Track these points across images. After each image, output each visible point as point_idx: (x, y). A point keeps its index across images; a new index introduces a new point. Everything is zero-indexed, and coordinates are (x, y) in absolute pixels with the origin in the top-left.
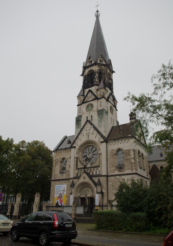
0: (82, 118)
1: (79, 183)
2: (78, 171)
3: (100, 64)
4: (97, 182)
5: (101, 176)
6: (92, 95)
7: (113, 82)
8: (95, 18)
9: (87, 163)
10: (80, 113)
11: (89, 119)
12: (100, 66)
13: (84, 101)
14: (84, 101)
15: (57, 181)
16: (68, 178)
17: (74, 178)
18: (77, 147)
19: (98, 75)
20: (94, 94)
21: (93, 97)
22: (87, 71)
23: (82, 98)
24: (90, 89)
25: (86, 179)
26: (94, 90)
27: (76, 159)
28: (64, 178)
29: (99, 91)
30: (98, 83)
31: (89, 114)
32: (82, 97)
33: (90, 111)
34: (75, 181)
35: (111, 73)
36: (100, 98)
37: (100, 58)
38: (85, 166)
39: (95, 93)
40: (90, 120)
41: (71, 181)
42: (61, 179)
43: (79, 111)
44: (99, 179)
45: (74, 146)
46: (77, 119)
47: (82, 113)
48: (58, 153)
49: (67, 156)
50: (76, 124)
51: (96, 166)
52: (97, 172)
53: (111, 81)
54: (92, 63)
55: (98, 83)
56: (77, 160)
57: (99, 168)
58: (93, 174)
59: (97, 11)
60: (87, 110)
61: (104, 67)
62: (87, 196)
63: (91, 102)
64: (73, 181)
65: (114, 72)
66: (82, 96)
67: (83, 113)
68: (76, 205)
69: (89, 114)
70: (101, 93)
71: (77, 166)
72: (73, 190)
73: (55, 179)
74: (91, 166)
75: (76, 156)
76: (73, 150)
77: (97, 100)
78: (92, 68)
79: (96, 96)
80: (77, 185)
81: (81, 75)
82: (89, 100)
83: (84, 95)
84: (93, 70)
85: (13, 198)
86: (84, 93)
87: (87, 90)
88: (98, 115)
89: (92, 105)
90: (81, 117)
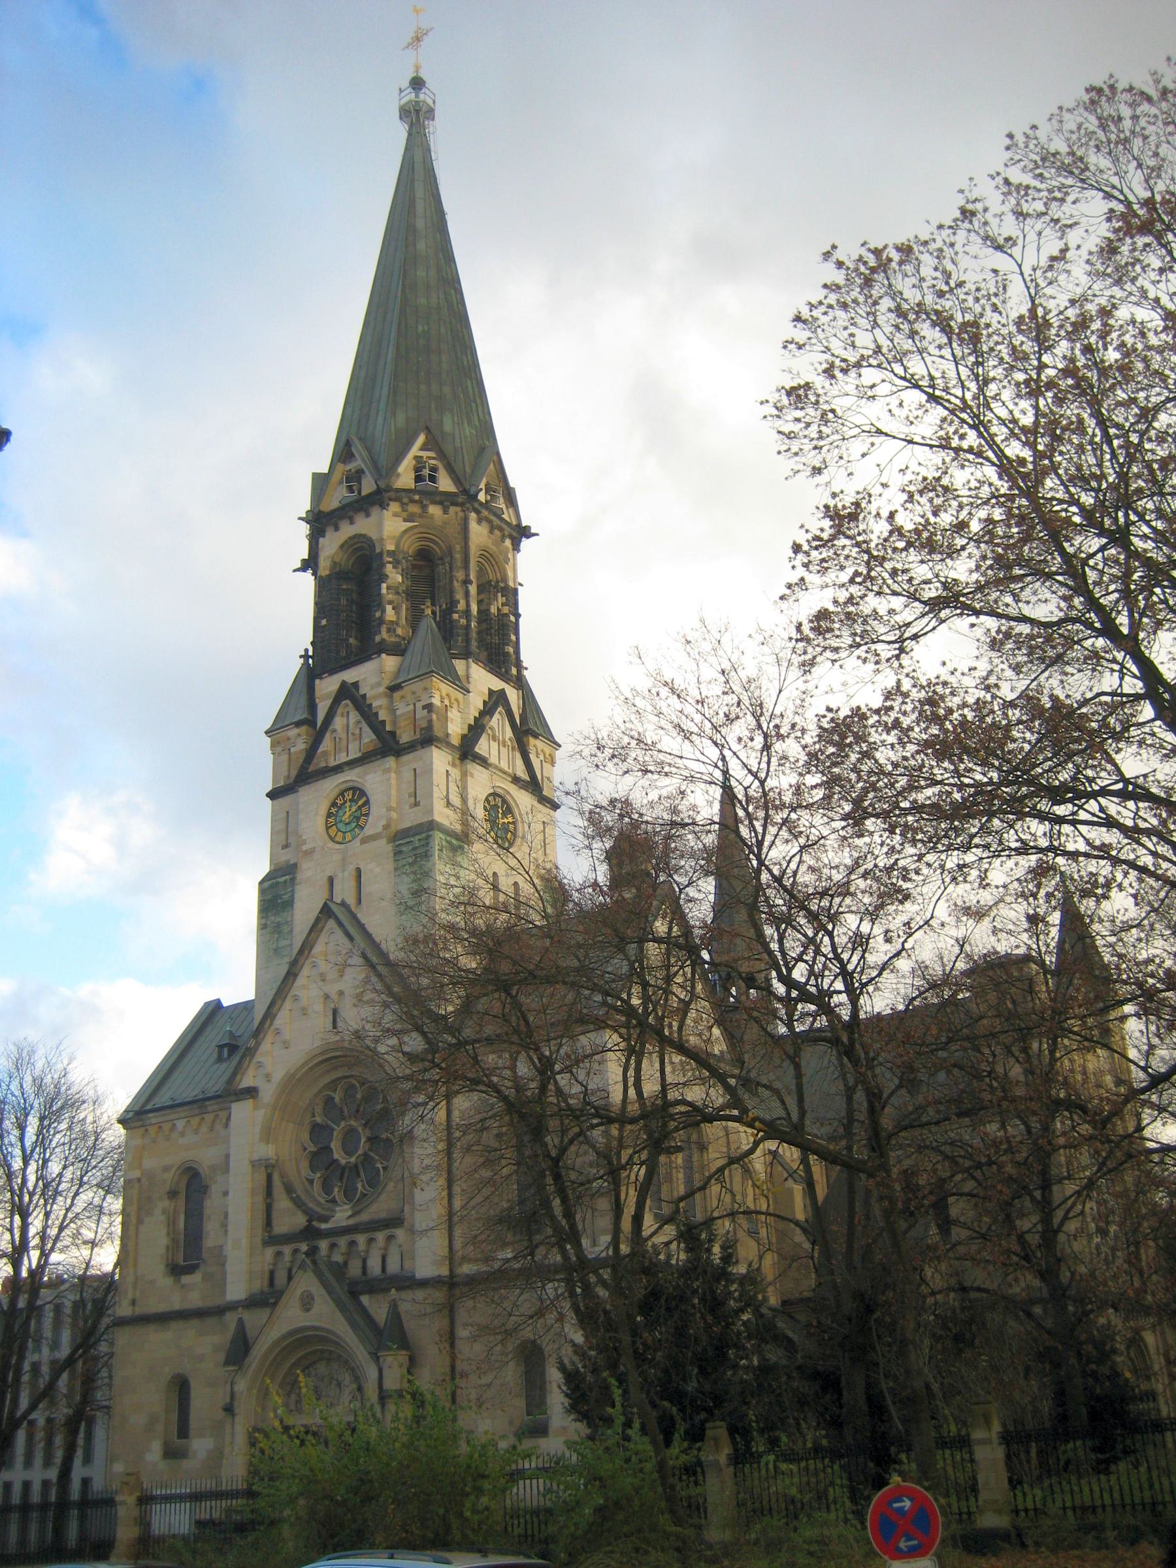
1: (275, 1333)
2: (279, 1254)
3: (417, 497)
4: (382, 1325)
5: (410, 1287)
6: (359, 722)
7: (520, 611)
8: (400, 132)
9: (334, 1201)
10: (286, 846)
11: (344, 891)
12: (414, 509)
13: (311, 768)
14: (311, 768)
16: (218, 1301)
17: (254, 1302)
18: (268, 1093)
19: (400, 579)
21: (369, 736)
22: (331, 544)
23: (299, 741)
25: (313, 1312)
26: (372, 688)
27: (262, 1177)
28: (195, 1300)
29: (407, 690)
30: (399, 631)
31: (337, 857)
33: (349, 836)
34: (253, 1319)
35: (508, 543)
36: (412, 747)
37: (415, 450)
38: (311, 1216)
39: (379, 704)
40: (351, 901)
41: (231, 1319)
44: (394, 1305)
45: (247, 1081)
46: (269, 897)
48: (152, 1130)
49: (206, 1157)
50: (262, 927)
51: (383, 1215)
52: (389, 1261)
53: (501, 599)
54: (364, 493)
55: (399, 631)
56: (269, 1177)
57: (400, 1233)
58: (369, 1272)
59: (417, 83)
60: (333, 831)
61: (446, 512)
63: (350, 776)
64: (241, 1322)
66: (298, 724)
67: (305, 848)
70: (419, 705)
71: (269, 1223)
72: (241, 1386)
74: (351, 1222)
75: (268, 1151)
76: (241, 1111)
77: (391, 762)
78: (362, 525)
79: (388, 728)
80: (265, 1347)
81: (299, 565)
82: (343, 758)
84: (370, 539)
85: (75, 1512)
86: (312, 707)
87: (328, 686)
89: (363, 793)
90: (293, 879)
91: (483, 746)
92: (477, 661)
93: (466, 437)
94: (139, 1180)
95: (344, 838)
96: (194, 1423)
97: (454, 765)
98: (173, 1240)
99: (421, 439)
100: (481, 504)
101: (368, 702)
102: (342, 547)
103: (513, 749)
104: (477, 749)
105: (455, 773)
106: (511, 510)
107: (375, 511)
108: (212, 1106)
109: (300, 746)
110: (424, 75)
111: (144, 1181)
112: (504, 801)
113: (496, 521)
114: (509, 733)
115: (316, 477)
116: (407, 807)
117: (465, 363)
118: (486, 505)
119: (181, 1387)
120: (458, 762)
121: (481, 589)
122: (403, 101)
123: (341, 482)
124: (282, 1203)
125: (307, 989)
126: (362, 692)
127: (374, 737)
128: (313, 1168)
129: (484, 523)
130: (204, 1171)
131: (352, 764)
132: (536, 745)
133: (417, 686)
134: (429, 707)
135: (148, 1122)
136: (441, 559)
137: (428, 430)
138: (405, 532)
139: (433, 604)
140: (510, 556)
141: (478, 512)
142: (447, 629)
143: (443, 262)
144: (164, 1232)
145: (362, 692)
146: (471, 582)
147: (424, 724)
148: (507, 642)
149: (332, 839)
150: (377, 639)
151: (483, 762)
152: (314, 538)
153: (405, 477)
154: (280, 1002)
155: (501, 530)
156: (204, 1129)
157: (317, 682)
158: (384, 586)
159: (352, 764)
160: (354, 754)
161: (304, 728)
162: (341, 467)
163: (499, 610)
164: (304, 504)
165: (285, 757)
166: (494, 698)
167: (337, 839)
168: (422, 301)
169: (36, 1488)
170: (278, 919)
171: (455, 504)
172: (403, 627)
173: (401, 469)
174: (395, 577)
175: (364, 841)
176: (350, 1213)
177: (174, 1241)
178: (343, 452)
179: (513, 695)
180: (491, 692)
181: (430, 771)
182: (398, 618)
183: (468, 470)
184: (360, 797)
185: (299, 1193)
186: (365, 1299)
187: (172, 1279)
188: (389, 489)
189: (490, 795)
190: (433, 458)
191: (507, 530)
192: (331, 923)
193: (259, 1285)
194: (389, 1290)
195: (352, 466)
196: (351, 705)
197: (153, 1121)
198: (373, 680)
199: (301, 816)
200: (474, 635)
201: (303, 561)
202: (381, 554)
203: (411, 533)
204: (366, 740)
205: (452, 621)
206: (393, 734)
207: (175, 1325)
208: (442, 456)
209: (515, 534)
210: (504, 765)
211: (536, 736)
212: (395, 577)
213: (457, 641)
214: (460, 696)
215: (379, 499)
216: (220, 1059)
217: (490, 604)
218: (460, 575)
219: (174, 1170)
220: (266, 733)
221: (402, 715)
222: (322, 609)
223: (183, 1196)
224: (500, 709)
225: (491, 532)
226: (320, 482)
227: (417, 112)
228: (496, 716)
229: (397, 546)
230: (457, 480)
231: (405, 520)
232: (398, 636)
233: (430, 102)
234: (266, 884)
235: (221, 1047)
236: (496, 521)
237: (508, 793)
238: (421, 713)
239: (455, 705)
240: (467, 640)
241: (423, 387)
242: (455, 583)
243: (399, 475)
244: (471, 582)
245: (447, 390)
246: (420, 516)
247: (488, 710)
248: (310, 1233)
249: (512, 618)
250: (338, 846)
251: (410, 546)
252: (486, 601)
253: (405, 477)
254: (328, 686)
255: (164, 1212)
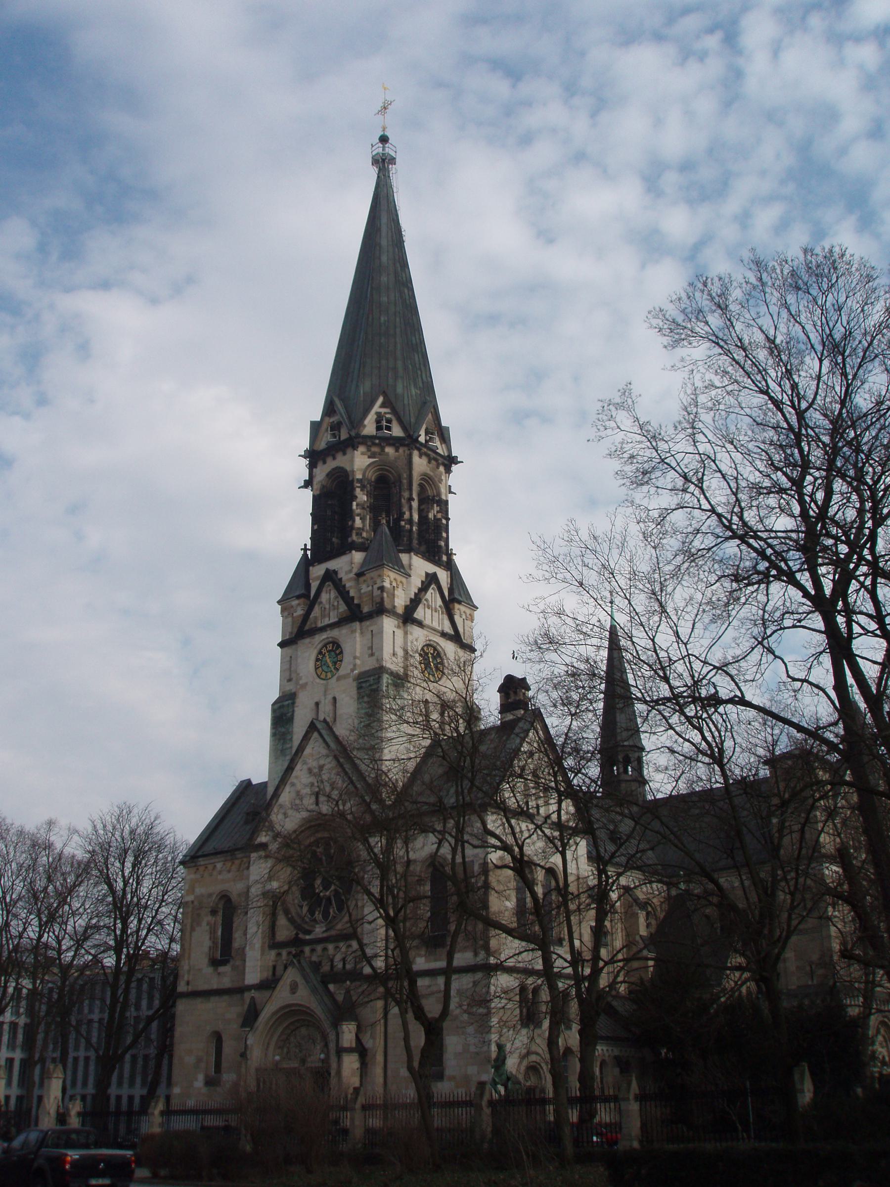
0: (296, 709)
2: (279, 954)
8: (372, 173)
10: (290, 680)
12: (375, 449)
13: (307, 628)
14: (307, 628)
15: (199, 1000)
19: (365, 498)
20: (348, 592)
21: (343, 607)
22: (321, 472)
24: (332, 565)
28: (227, 983)
29: (368, 575)
30: (364, 535)
32: (299, 604)
33: (329, 675)
35: (442, 469)
36: (370, 616)
37: (376, 408)
41: (248, 996)
42: (215, 987)
43: (289, 672)
47: (297, 683)
48: (201, 869)
49: (235, 889)
50: (274, 735)
53: (436, 508)
59: (384, 140)
61: (397, 451)
62: (309, 1065)
63: (335, 633)
65: (457, 463)
66: (298, 597)
67: (301, 682)
68: (162, 1109)
69: (325, 691)
73: (190, 990)
74: (325, 935)
77: (357, 625)
78: (340, 461)
79: (356, 601)
82: (326, 621)
83: (306, 596)
84: (346, 471)
86: (308, 586)
87: (318, 571)
88: (358, 699)
89: (339, 646)
90: (293, 703)
91: (419, 614)
92: (416, 554)
93: (412, 396)
94: (193, 902)
95: (326, 676)
96: (224, 1065)
97: (398, 627)
98: (213, 942)
99: (381, 400)
100: (421, 444)
101: (343, 583)
102: (328, 475)
103: (442, 613)
104: (415, 615)
105: (399, 633)
106: (443, 445)
107: (349, 451)
108: (239, 855)
109: (300, 612)
110: (387, 134)
111: (196, 903)
112: (435, 649)
113: (432, 455)
114: (439, 602)
115: (313, 424)
116: (367, 656)
117: (414, 342)
118: (426, 445)
119: (218, 1038)
120: (401, 624)
121: (421, 502)
122: (374, 153)
123: (327, 430)
124: (282, 921)
125: (301, 776)
126: (339, 576)
127: (346, 608)
128: (304, 898)
129: (424, 457)
130: (234, 897)
131: (332, 626)
132: (459, 610)
133: (374, 574)
134: (382, 589)
135: (199, 863)
136: (394, 483)
137: (385, 394)
138: (369, 465)
139: (388, 516)
140: (443, 478)
141: (419, 450)
142: (397, 532)
143: (399, 269)
144: (208, 937)
145: (339, 576)
146: (413, 500)
147: (378, 600)
148: (440, 537)
149: (319, 677)
150: (350, 540)
151: (420, 624)
152: (312, 466)
153: (369, 427)
154: (282, 787)
155: (436, 460)
156: (234, 868)
157: (311, 568)
158: (354, 503)
159: (332, 626)
160: (334, 619)
161: (302, 600)
162: (327, 419)
163: (435, 516)
164: (304, 443)
165: (290, 619)
166: (429, 579)
167: (322, 677)
168: (384, 299)
169: (125, 1101)
170: (283, 730)
171: (404, 445)
172: (367, 532)
173: (366, 422)
174: (362, 497)
175: (338, 679)
176: (324, 929)
177: (215, 943)
178: (329, 409)
179: (443, 576)
180: (427, 574)
181: (381, 632)
182: (364, 526)
183: (413, 420)
184: (337, 648)
185: (294, 914)
186: (331, 987)
187: (212, 968)
188: (358, 436)
189: (424, 646)
190: (388, 413)
191: (441, 460)
192: (316, 734)
193: (267, 974)
194: (345, 981)
195: (334, 419)
196: (332, 586)
197: (202, 863)
198: (346, 568)
199: (299, 660)
200: (415, 536)
201: (305, 481)
202: (353, 481)
203: (370, 468)
204: (341, 610)
205: (400, 526)
206: (359, 606)
207: (214, 999)
208: (394, 412)
209: (446, 462)
210: (435, 625)
211: (459, 602)
212: (362, 497)
213: (403, 540)
214: (404, 580)
215: (352, 443)
216: (247, 822)
217: (428, 512)
218: (406, 494)
219: (215, 896)
220: (279, 602)
221: (365, 593)
222: (317, 516)
223: (221, 913)
224: (433, 586)
225: (429, 462)
226: (315, 427)
227: (383, 161)
228: (430, 591)
229: (364, 475)
230: (404, 428)
231: (369, 457)
232: (363, 538)
233: (393, 154)
234: (276, 706)
235: (248, 814)
236: (432, 455)
237: (437, 643)
238: (377, 593)
239: (400, 586)
240: (410, 540)
241: (383, 362)
242: (403, 500)
243: (365, 426)
244: (413, 500)
245: (400, 364)
246: (380, 454)
247: (424, 588)
248: (296, 942)
249: (444, 521)
250: (322, 682)
251: (372, 475)
252: (426, 510)
253: (369, 427)
254: (318, 571)
255: (208, 924)
